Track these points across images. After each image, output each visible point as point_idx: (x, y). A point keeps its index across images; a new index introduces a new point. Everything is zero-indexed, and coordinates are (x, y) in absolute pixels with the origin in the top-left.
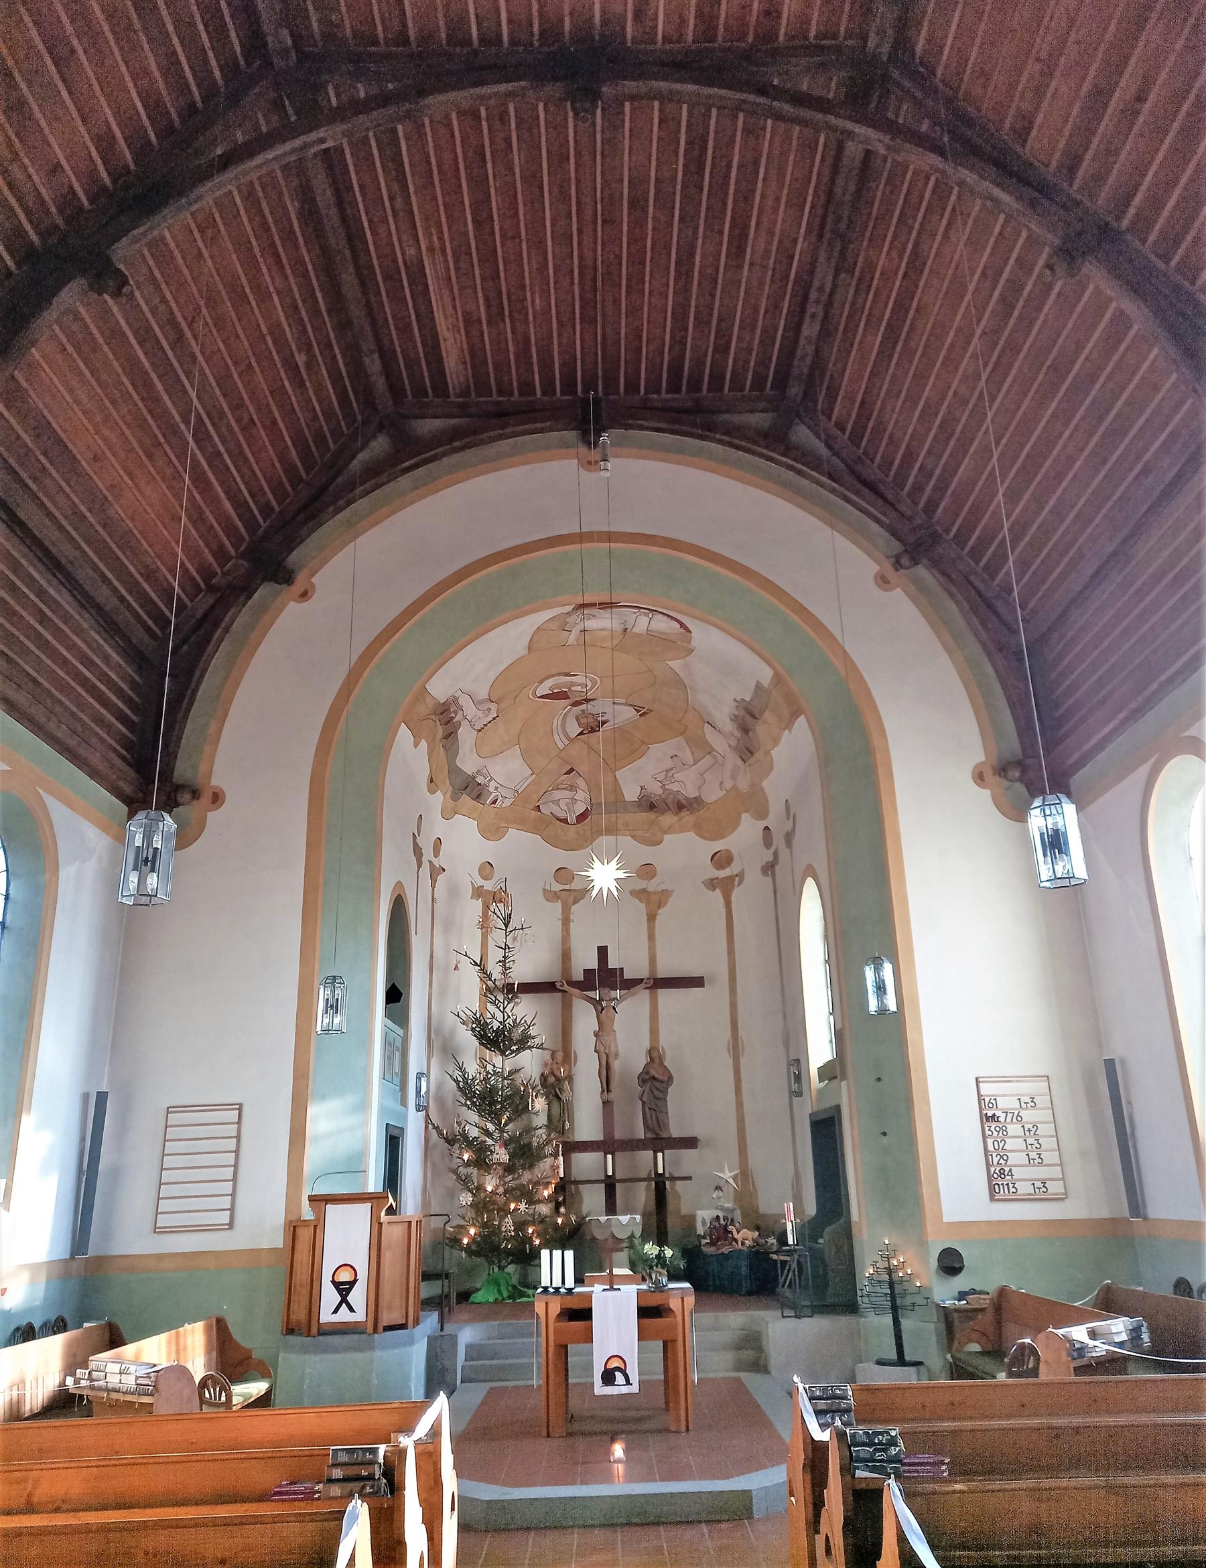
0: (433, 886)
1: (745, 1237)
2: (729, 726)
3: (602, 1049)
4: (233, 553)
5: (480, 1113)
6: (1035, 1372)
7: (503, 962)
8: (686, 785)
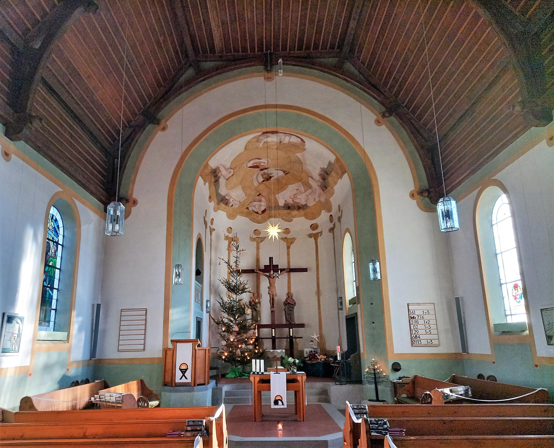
0: (211, 235)
1: (321, 358)
2: (318, 178)
3: (271, 293)
4: (138, 113)
5: (228, 314)
6: (431, 403)
7: (236, 262)
8: (301, 200)
